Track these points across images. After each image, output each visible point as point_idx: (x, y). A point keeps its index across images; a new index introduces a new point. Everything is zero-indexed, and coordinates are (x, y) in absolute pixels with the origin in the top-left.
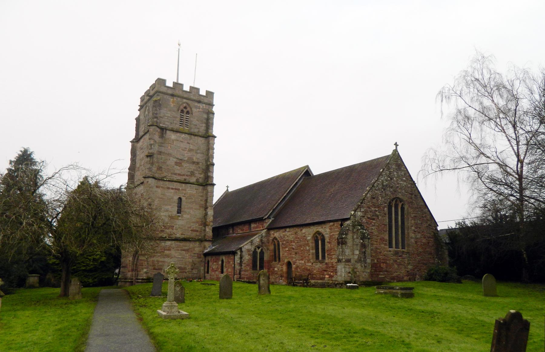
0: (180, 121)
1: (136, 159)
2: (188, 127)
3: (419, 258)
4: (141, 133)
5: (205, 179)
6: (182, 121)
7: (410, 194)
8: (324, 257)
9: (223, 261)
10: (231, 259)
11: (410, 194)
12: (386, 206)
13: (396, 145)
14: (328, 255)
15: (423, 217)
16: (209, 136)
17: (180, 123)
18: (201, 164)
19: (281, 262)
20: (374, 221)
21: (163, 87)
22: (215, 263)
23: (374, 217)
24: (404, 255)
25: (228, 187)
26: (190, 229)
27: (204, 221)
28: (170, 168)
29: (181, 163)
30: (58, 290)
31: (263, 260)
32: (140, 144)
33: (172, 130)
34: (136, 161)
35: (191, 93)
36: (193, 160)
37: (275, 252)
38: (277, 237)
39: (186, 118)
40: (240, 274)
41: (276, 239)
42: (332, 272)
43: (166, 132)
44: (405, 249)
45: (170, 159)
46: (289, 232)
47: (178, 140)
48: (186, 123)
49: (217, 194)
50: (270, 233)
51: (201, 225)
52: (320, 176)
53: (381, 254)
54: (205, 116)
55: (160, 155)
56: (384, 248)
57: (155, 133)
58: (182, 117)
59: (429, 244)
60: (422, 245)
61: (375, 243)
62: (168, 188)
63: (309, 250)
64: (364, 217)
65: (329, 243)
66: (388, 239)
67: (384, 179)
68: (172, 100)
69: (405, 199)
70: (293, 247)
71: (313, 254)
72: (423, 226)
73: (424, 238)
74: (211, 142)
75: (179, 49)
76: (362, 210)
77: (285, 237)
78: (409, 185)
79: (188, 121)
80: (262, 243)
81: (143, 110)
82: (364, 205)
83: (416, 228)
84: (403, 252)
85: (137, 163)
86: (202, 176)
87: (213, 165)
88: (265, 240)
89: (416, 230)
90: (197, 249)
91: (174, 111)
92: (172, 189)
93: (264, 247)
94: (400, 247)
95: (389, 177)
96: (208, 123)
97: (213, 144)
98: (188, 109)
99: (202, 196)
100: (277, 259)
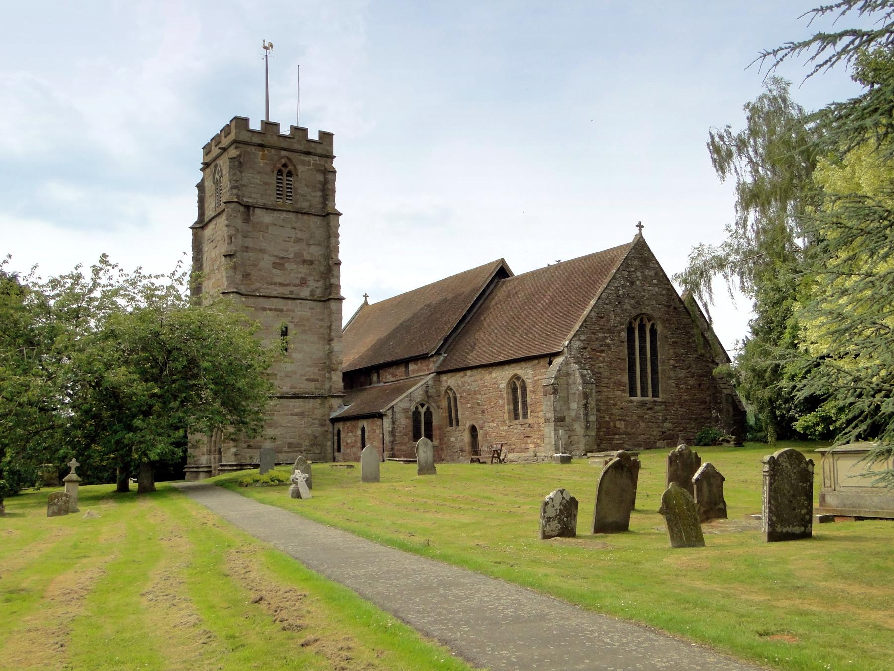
0: (277, 190)
1: (202, 259)
2: (290, 200)
3: (683, 409)
4: (209, 213)
5: (326, 289)
6: (281, 189)
7: (665, 306)
8: (525, 415)
9: (363, 430)
10: (377, 426)
11: (665, 306)
12: (623, 329)
13: (640, 226)
14: (532, 411)
15: (688, 343)
16: (328, 214)
17: (278, 194)
18: (317, 263)
19: (460, 427)
20: (603, 355)
21: (244, 133)
22: (350, 434)
23: (602, 348)
24: (655, 407)
25: (366, 296)
26: (305, 378)
27: (328, 363)
28: (265, 274)
29: (283, 265)
30: (113, 487)
31: (432, 426)
32: (208, 232)
33: (265, 208)
34: (202, 262)
35: (293, 138)
36: (303, 256)
37: (450, 412)
38: (452, 387)
39: (287, 184)
40: (392, 449)
41: (451, 389)
42: (539, 438)
43: (254, 211)
44: (658, 397)
45: (263, 259)
46: (471, 376)
47: (276, 225)
48: (287, 192)
49: (349, 310)
50: (441, 378)
51: (323, 370)
52: (523, 277)
53: (617, 407)
54: (320, 178)
55: (247, 252)
56: (622, 397)
57: (236, 215)
58: (279, 182)
59: (702, 387)
60: (688, 388)
61: (606, 389)
62: (264, 309)
63: (503, 406)
64: (585, 348)
65: (534, 392)
66: (628, 382)
67: (619, 285)
68: (261, 153)
69: (656, 314)
70: (479, 401)
71: (509, 412)
72: (689, 357)
73: (692, 377)
74: (332, 223)
75: (266, 56)
76: (582, 338)
77: (464, 386)
78: (664, 292)
79: (291, 189)
80: (428, 397)
81: (208, 170)
82: (586, 329)
83: (677, 361)
84: (655, 401)
85: (204, 265)
86: (320, 284)
87: (338, 264)
88: (431, 391)
89: (676, 365)
90: (318, 411)
91: (266, 174)
92: (271, 310)
93: (432, 404)
94: (650, 393)
95: (628, 281)
96: (327, 190)
97: (338, 226)
98: (290, 167)
99: (322, 320)
100: (454, 423)
